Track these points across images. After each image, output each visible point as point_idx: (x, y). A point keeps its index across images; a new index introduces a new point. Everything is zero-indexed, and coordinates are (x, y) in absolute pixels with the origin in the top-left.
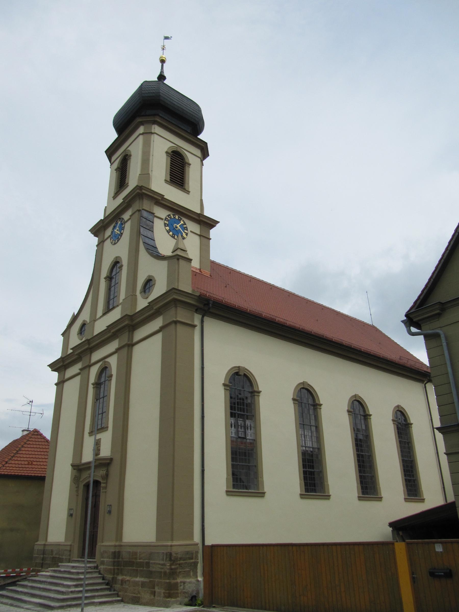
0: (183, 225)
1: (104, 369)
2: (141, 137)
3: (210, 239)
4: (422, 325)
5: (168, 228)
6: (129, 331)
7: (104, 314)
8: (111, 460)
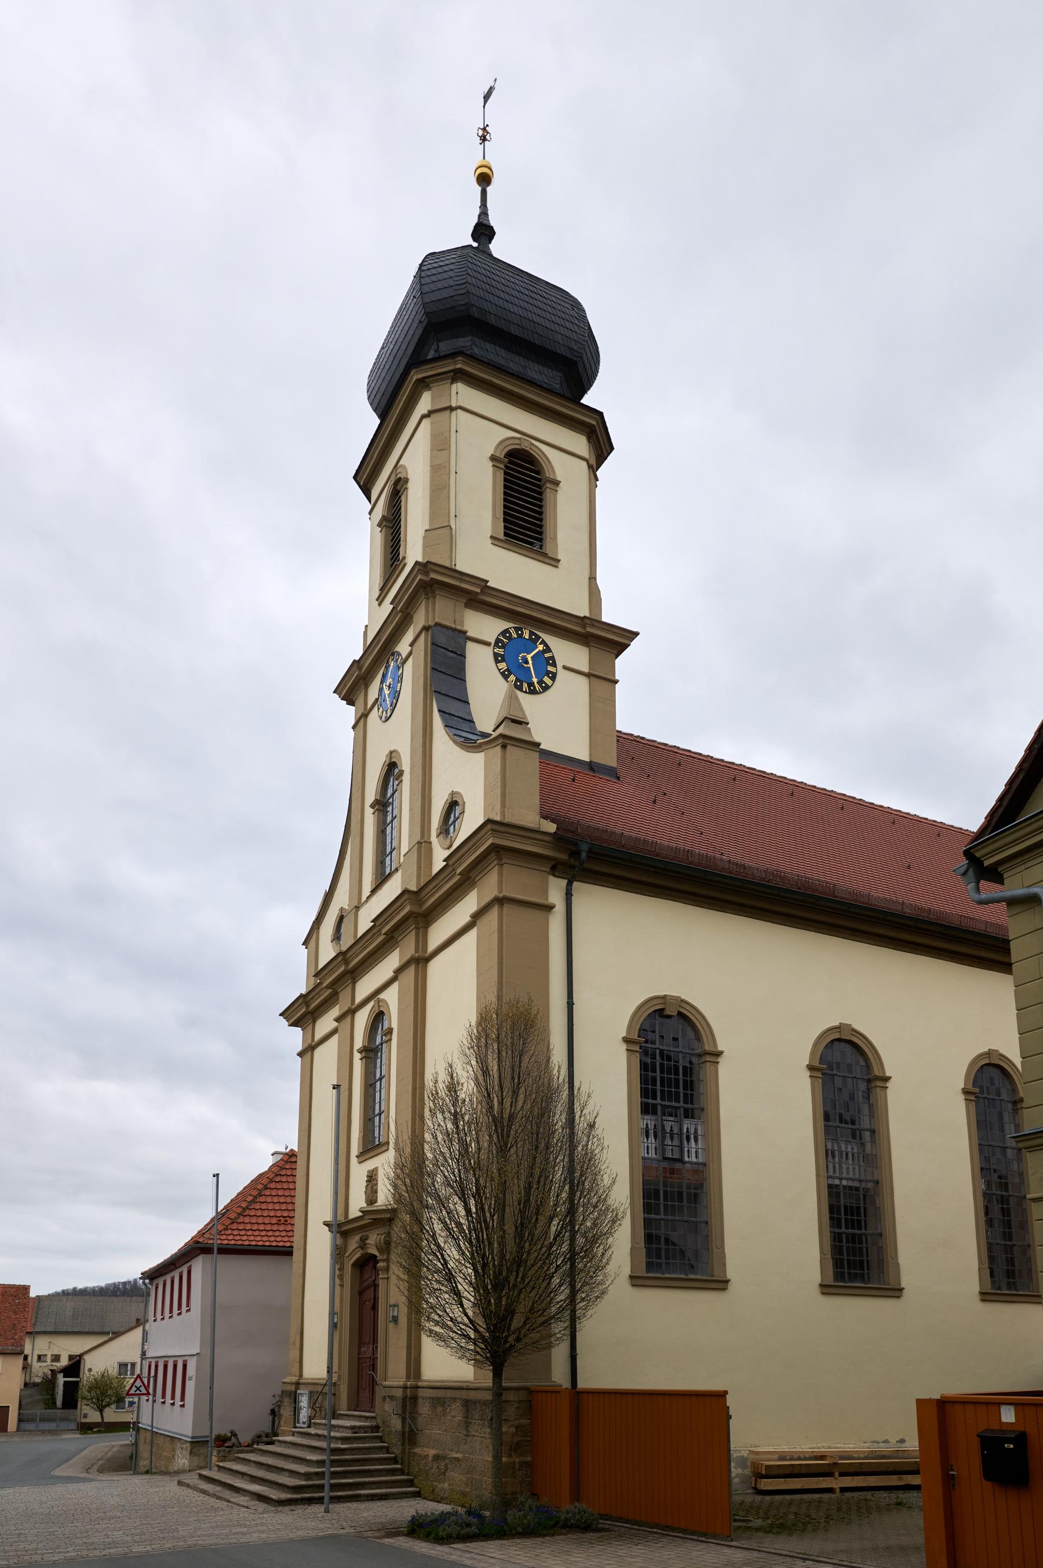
0: (544, 652)
1: (378, 1017)
2: (426, 423)
3: (616, 682)
4: (1005, 876)
5: (503, 666)
6: (417, 928)
7: (374, 891)
8: (394, 1211)
